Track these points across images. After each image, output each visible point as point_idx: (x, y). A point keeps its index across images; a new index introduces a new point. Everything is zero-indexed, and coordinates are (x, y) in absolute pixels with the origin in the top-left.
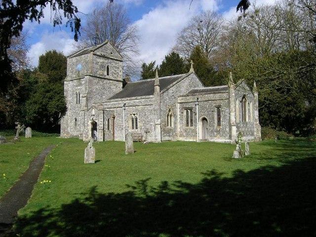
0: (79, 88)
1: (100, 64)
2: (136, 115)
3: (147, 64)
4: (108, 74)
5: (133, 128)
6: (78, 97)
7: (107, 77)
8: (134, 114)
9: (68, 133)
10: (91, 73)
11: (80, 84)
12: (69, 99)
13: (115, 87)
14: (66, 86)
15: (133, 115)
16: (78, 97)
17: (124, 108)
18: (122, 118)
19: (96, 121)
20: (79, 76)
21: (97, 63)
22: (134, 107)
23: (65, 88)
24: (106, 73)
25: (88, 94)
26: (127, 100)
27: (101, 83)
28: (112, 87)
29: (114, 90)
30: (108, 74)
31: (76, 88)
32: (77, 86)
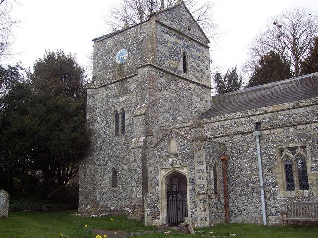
0: (122, 99)
1: (169, 44)
2: (299, 151)
3: (223, 74)
4: (185, 71)
5: (290, 187)
6: (120, 120)
7: (183, 75)
8: (293, 149)
9: (95, 204)
10: (152, 61)
11: (127, 91)
12: (98, 126)
13: (198, 99)
14: (92, 99)
15: (287, 152)
16: (120, 120)
17: (256, 133)
18: (254, 161)
19: (184, 171)
20: (120, 75)
21: (165, 42)
22: (291, 130)
23: (89, 103)
24: (181, 68)
25: (148, 107)
26: (266, 112)
27: (174, 87)
28: (195, 99)
29: (198, 105)
30: (185, 71)
31: (116, 101)
32: (117, 97)
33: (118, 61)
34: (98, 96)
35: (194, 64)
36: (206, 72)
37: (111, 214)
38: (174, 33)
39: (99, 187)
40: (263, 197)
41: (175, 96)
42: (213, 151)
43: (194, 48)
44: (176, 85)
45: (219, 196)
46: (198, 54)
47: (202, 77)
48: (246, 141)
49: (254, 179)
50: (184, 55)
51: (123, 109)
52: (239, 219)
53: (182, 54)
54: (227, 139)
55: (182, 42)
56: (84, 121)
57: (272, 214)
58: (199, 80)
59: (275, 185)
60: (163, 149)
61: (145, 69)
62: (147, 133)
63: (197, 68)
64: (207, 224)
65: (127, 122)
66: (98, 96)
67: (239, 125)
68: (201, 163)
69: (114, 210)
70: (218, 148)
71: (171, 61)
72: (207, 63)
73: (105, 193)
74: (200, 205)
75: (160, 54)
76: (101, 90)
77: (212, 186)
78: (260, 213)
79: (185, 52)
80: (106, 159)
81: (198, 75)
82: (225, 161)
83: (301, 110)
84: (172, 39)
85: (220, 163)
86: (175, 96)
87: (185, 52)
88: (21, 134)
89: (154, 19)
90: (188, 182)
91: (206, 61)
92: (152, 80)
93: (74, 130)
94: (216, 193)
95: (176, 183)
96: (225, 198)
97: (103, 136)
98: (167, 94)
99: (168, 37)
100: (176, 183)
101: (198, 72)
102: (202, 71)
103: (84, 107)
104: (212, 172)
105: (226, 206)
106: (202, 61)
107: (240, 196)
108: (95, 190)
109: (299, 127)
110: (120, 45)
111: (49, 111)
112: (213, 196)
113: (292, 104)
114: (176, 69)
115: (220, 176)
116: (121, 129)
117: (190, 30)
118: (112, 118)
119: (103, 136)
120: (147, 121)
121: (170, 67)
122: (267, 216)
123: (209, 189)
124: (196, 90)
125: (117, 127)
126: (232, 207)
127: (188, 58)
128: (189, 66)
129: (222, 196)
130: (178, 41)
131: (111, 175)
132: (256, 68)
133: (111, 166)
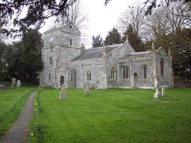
0: (52, 53)
1: (65, 37)
4: (71, 44)
5: (88, 80)
7: (70, 46)
8: (89, 71)
9: (44, 84)
10: (59, 44)
11: (53, 51)
12: (45, 61)
15: (88, 72)
17: (82, 67)
19: (64, 76)
20: (51, 46)
21: (64, 37)
22: (89, 66)
24: (69, 44)
25: (58, 57)
26: (84, 61)
27: (67, 50)
28: (74, 53)
29: (75, 55)
30: (71, 44)
32: (50, 52)
33: (50, 41)
34: (45, 52)
37: (48, 86)
38: (67, 33)
41: (67, 53)
42: (71, 71)
46: (76, 38)
52: (78, 87)
53: (70, 40)
54: (76, 67)
55: (70, 36)
56: (41, 59)
59: (85, 79)
60: (59, 70)
61: (57, 46)
62: (57, 65)
64: (68, 88)
65: (53, 60)
66: (45, 52)
67: (79, 64)
68: (67, 74)
69: (50, 86)
72: (79, 40)
74: (66, 84)
75: (62, 41)
76: (46, 50)
79: (71, 39)
81: (76, 45)
82: (75, 73)
83: (91, 62)
84: (67, 35)
86: (67, 53)
87: (71, 39)
88: (22, 64)
89: (60, 30)
92: (59, 49)
93: (38, 62)
94: (72, 81)
95: (62, 78)
96: (74, 82)
98: (64, 53)
99: (65, 35)
100: (62, 78)
103: (41, 55)
105: (75, 84)
109: (90, 66)
110: (51, 36)
111: (30, 56)
113: (90, 60)
114: (67, 45)
116: (51, 63)
118: (49, 59)
120: (57, 62)
121: (65, 44)
125: (50, 62)
126: (77, 85)
127: (72, 40)
128: (72, 43)
130: (68, 35)
132: (130, 26)
133: (49, 73)
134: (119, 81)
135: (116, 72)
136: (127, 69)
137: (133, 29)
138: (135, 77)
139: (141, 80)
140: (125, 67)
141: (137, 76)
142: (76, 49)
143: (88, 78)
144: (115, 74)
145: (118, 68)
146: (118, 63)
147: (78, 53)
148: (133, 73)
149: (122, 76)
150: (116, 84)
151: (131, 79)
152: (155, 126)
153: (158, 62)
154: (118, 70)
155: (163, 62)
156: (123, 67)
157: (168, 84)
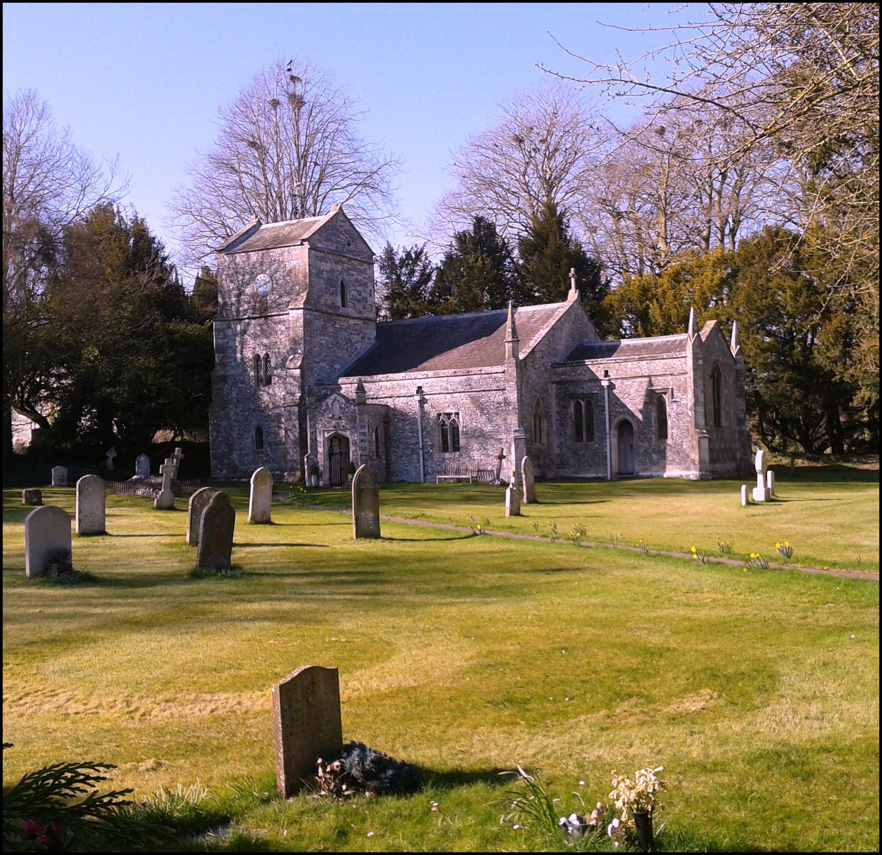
1: (325, 275)
7: (341, 310)
8: (449, 415)
24: (339, 304)
27: (331, 329)
28: (355, 338)
29: (359, 346)
30: (343, 306)
35: (354, 293)
36: (369, 299)
39: (237, 448)
40: (421, 458)
41: (332, 340)
43: (355, 269)
44: (333, 325)
45: (380, 457)
47: (364, 308)
48: (71, 321)
49: (414, 441)
50: (342, 282)
51: (267, 355)
53: (339, 283)
55: (339, 268)
57: (429, 474)
58: (360, 312)
59: (432, 446)
63: (358, 297)
70: (580, 760)
71: (327, 296)
73: (247, 455)
77: (374, 448)
78: (419, 474)
80: (246, 414)
81: (360, 306)
85: (382, 424)
90: (351, 445)
91: (369, 284)
96: (386, 459)
97: (240, 385)
101: (359, 301)
102: (365, 299)
104: (374, 434)
105: (388, 466)
106: (365, 285)
107: (402, 457)
108: (231, 451)
109: (455, 395)
112: (375, 457)
115: (382, 439)
117: (349, 245)
119: (240, 385)
122: (425, 475)
123: (370, 451)
124: (356, 327)
127: (346, 287)
129: (383, 457)
130: (334, 266)
131: (254, 432)
133: (254, 423)
134: (557, 451)
135: (548, 415)
136: (589, 404)
137: (847, 409)
138: (620, 436)
139: (646, 445)
140: (583, 396)
141: (632, 434)
142: (361, 322)
143: (445, 442)
144: (545, 424)
145: (554, 401)
146: (553, 383)
147: (369, 339)
148: (616, 420)
149: (570, 430)
150: (547, 461)
151: (608, 440)
152: (785, 158)
153: (707, 378)
154: (554, 408)
155: (719, 374)
156: (575, 396)
157: (734, 459)
